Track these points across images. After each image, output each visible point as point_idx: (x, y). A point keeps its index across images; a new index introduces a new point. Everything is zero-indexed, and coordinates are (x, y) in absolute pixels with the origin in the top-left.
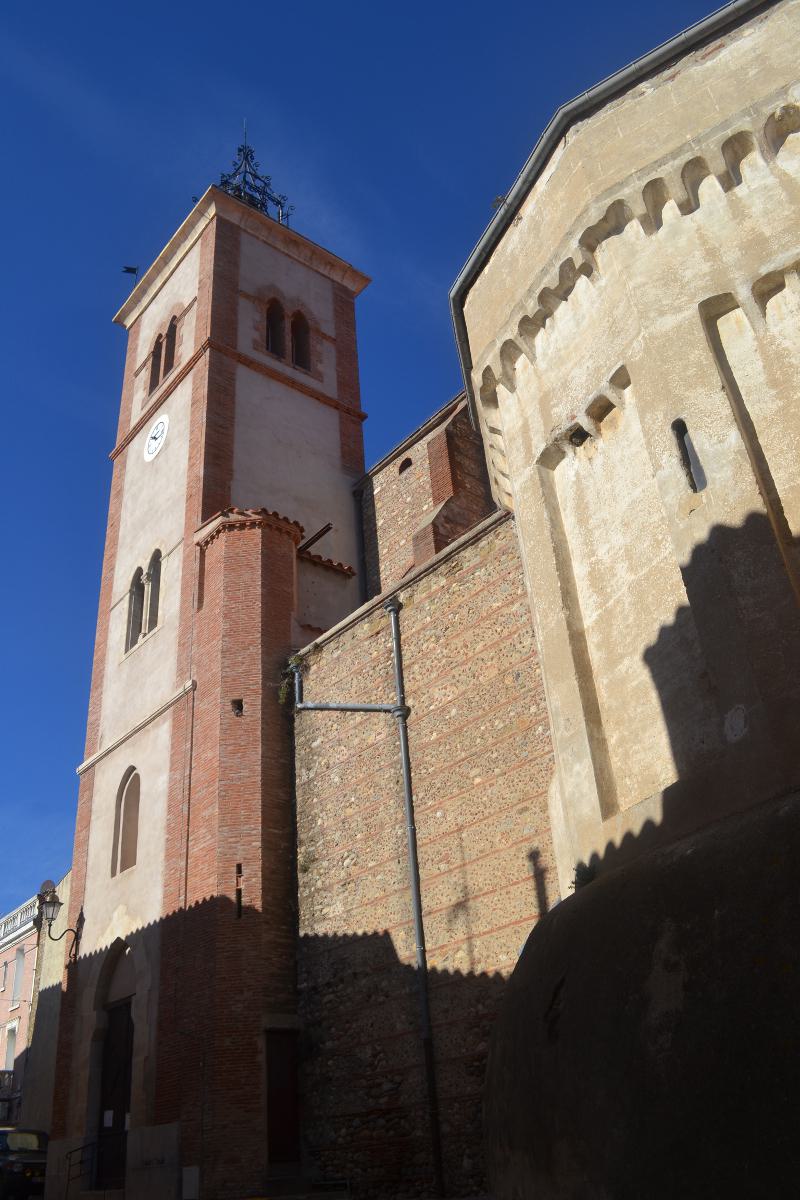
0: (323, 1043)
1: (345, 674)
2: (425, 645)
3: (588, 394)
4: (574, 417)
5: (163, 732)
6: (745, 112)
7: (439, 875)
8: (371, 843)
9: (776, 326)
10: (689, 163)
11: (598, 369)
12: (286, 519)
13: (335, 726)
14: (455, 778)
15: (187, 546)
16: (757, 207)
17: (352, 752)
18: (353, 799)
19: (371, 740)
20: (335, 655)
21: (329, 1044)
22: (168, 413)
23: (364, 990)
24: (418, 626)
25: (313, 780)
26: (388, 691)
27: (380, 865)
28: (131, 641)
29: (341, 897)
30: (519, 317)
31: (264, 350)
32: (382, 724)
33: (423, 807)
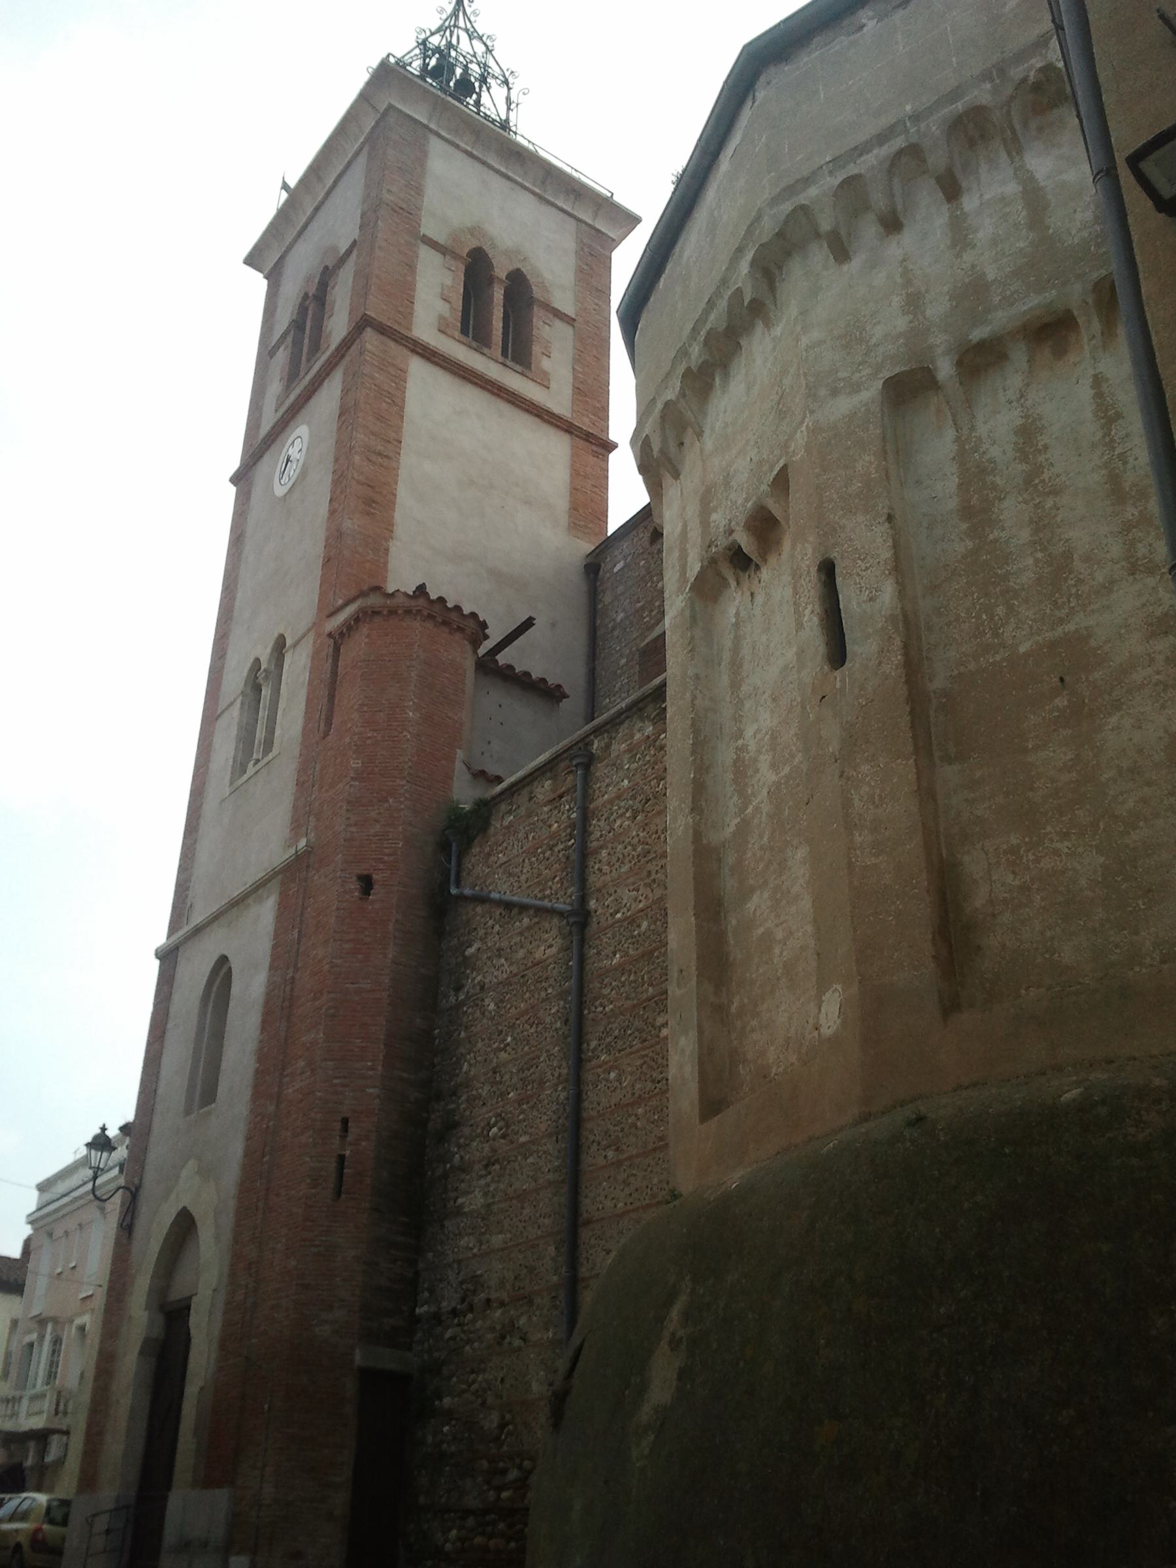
0: (440, 1399)
1: (515, 852)
2: (618, 823)
3: (747, 500)
4: (731, 532)
5: (265, 912)
6: (986, 76)
7: (605, 1167)
8: (525, 1106)
9: (985, 423)
10: (900, 153)
11: (760, 463)
12: (458, 608)
13: (497, 927)
14: (638, 1023)
15: (318, 635)
16: (985, 230)
17: (514, 969)
18: (509, 1039)
19: (538, 955)
20: (506, 823)
21: (447, 1401)
22: (309, 424)
23: (498, 1327)
24: (612, 791)
25: (463, 1003)
26: (566, 884)
27: (532, 1142)
28: (240, 768)
29: (482, 1182)
30: (681, 370)
31: (457, 334)
32: (554, 932)
33: (594, 1062)
